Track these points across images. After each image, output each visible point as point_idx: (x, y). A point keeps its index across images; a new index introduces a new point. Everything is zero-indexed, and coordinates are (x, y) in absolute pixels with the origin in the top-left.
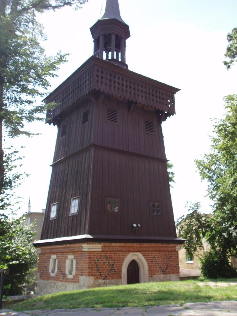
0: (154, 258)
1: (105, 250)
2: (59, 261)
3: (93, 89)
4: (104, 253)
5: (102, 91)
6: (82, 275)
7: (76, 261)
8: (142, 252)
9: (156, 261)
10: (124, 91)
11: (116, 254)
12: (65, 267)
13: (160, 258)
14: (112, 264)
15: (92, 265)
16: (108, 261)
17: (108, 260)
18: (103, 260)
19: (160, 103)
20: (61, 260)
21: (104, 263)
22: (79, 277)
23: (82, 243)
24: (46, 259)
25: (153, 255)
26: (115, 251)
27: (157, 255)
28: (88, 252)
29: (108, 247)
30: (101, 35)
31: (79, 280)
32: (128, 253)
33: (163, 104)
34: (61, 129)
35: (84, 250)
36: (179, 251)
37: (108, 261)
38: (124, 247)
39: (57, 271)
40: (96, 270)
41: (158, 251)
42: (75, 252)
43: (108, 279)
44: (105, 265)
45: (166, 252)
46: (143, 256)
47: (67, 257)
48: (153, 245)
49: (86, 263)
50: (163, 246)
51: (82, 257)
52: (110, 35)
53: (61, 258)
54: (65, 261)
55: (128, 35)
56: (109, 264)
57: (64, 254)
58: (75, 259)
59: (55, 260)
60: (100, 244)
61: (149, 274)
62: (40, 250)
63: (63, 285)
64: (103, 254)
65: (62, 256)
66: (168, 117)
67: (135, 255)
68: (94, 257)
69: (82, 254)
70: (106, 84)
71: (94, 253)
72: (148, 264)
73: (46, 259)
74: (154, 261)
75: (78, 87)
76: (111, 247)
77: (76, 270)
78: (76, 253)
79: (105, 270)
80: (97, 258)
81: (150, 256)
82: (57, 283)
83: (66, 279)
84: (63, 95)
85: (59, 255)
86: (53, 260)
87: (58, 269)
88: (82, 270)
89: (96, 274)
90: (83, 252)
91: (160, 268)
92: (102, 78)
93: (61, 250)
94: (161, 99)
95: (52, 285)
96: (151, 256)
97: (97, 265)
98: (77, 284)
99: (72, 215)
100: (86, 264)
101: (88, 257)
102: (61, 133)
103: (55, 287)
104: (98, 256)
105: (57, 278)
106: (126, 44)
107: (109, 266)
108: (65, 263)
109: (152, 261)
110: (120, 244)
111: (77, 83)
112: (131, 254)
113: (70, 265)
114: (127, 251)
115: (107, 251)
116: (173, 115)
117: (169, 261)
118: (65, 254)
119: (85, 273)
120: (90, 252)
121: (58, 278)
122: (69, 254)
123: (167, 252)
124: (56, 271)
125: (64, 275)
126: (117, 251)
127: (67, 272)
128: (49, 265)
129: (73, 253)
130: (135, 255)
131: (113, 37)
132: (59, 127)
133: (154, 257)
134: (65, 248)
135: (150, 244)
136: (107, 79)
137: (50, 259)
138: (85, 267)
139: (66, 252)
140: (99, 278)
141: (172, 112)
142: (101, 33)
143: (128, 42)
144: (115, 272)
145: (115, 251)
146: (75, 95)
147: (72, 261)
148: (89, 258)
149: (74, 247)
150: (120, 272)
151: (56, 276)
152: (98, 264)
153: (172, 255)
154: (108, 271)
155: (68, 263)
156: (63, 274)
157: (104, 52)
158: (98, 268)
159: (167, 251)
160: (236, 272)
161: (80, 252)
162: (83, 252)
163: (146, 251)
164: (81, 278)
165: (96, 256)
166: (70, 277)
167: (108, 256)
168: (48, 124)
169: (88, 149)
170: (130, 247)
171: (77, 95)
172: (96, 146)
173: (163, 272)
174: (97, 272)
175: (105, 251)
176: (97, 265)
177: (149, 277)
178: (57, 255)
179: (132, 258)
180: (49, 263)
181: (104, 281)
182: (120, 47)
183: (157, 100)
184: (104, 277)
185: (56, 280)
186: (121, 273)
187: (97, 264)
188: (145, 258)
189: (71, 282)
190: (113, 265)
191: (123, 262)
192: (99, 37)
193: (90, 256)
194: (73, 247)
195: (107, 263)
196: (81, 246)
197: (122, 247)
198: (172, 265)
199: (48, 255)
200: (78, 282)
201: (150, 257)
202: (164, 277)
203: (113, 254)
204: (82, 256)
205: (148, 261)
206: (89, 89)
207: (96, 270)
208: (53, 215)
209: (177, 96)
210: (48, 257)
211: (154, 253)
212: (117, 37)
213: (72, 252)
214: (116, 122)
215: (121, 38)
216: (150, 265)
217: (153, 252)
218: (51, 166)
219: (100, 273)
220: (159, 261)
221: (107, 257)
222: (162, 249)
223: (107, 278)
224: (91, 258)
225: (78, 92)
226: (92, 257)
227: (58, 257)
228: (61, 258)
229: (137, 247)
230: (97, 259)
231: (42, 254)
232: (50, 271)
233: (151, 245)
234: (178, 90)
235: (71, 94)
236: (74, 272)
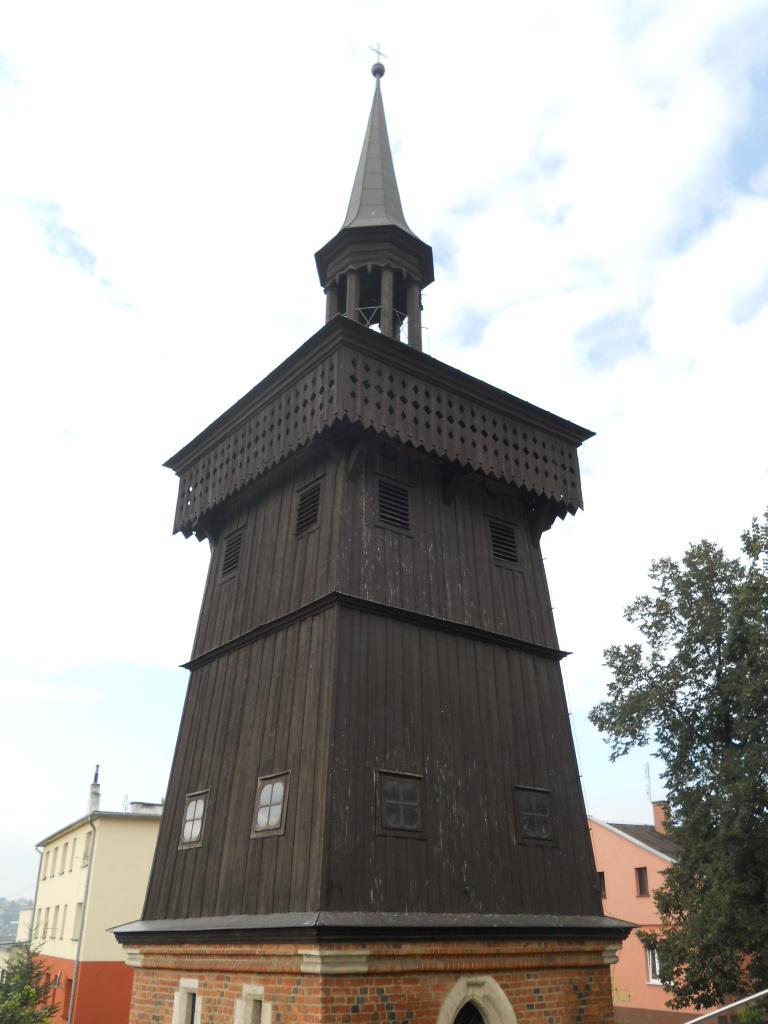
0: (537, 995)
2: (209, 1001)
3: (341, 418)
5: (367, 425)
7: (275, 1008)
8: (499, 974)
9: (543, 1006)
10: (433, 428)
13: (554, 993)
19: (537, 470)
20: (217, 997)
23: (300, 946)
25: (533, 983)
30: (350, 270)
32: (453, 977)
33: (547, 474)
34: (223, 553)
36: (612, 966)
42: (271, 973)
46: (503, 987)
47: (239, 989)
48: (534, 946)
51: (299, 995)
52: (377, 271)
53: (215, 993)
54: (232, 1004)
55: (428, 278)
57: (228, 979)
58: (268, 999)
59: (194, 995)
60: (364, 947)
64: (370, 982)
65: (219, 982)
66: (558, 519)
68: (340, 996)
69: (299, 983)
73: (162, 990)
75: (288, 417)
78: (273, 977)
80: (350, 1000)
81: (523, 988)
84: (236, 442)
85: (210, 978)
86: (186, 996)
90: (303, 974)
93: (216, 963)
94: (540, 460)
96: (528, 988)
99: (260, 835)
102: (222, 562)
106: (423, 302)
108: (231, 1012)
109: (530, 1007)
110: (429, 946)
111: (283, 403)
112: (463, 981)
116: (573, 512)
118: (231, 976)
122: (247, 981)
128: (169, 1013)
129: (261, 977)
131: (387, 281)
132: (214, 543)
133: (537, 991)
134: (236, 955)
135: (523, 944)
136: (381, 391)
137: (172, 991)
141: (568, 502)
142: (351, 267)
143: (428, 294)
146: (275, 439)
147: (258, 1004)
162: (299, 977)
167: (388, 990)
168: (180, 534)
169: (315, 609)
171: (282, 438)
172: (348, 604)
178: (201, 978)
179: (466, 996)
180: (171, 1005)
182: (407, 304)
183: (518, 467)
188: (508, 994)
191: (437, 1013)
192: (343, 279)
199: (168, 977)
201: (524, 992)
203: (407, 982)
204: (296, 991)
206: (325, 418)
208: (192, 830)
209: (585, 452)
210: (169, 984)
212: (397, 275)
213: (259, 973)
214: (407, 525)
215: (409, 279)
217: (532, 973)
220: (550, 1006)
221: (385, 994)
222: (560, 961)
224: (331, 1001)
225: (288, 431)
228: (215, 993)
230: (351, 1005)
233: (525, 946)
234: (588, 434)
235: (261, 439)
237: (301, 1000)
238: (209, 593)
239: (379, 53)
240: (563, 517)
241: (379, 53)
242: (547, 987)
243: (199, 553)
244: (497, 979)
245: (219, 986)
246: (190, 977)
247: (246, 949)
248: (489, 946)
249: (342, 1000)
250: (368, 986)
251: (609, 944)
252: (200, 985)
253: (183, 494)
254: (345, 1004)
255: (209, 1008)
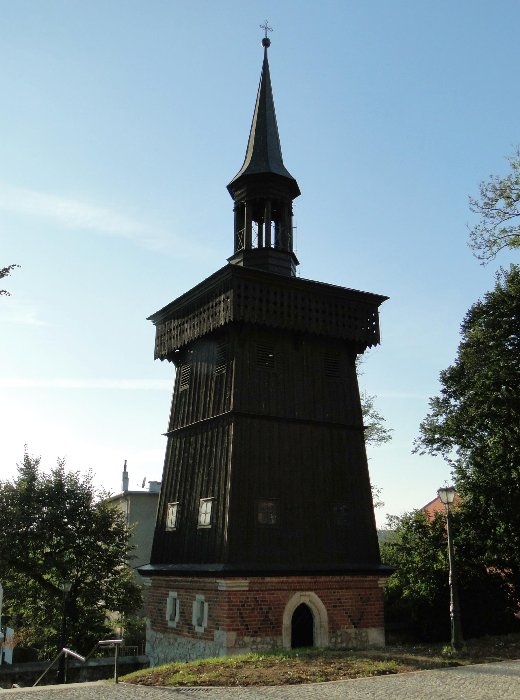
1: (254, 588)
4: (253, 593)
6: (218, 629)
7: (209, 605)
8: (317, 591)
11: (273, 594)
12: (191, 614)
14: (266, 611)
15: (233, 613)
16: (259, 607)
17: (260, 605)
18: (250, 605)
21: (253, 609)
22: (213, 632)
24: (161, 596)
25: (337, 596)
26: (272, 590)
27: (345, 595)
28: (227, 593)
29: (259, 583)
31: (213, 636)
32: (293, 592)
35: (219, 588)
37: (259, 607)
38: (286, 582)
39: (180, 619)
40: (240, 621)
41: (346, 588)
42: (207, 590)
43: (260, 636)
44: (254, 613)
45: (360, 590)
46: (319, 597)
47: (195, 597)
49: (224, 610)
50: (354, 579)
54: (192, 603)
56: (261, 611)
58: (206, 601)
60: (247, 579)
61: (330, 628)
62: (151, 581)
63: (190, 642)
67: (305, 596)
70: (253, 308)
71: (235, 594)
72: (328, 610)
73: (161, 596)
74: (339, 606)
76: (264, 583)
77: (208, 619)
78: (208, 592)
79: (255, 621)
80: (241, 602)
82: (178, 639)
83: (193, 633)
85: (182, 592)
87: (181, 616)
88: (218, 620)
89: (239, 627)
90: (219, 591)
91: (350, 616)
92: (246, 297)
95: (171, 641)
97: (241, 613)
98: (211, 643)
100: (224, 612)
101: (227, 600)
103: (177, 645)
104: (243, 598)
105: (178, 631)
107: (261, 614)
108: (191, 607)
112: (298, 594)
113: (199, 611)
114: (291, 589)
115: (257, 591)
117: (367, 605)
118: (191, 591)
119: (222, 625)
120: (230, 592)
121: (180, 631)
122: (197, 593)
123: (363, 590)
124: (177, 618)
125: (191, 628)
126: (275, 590)
127: (194, 622)
130: (305, 596)
133: (339, 599)
134: (192, 582)
135: (330, 577)
138: (223, 617)
139: (193, 589)
140: (245, 635)
141: (374, 339)
144: (271, 623)
145: (272, 590)
148: (227, 602)
149: (205, 582)
150: (279, 623)
151: (177, 626)
152: (243, 612)
153: (371, 594)
154: (260, 623)
155: (196, 606)
156: (188, 624)
157: (253, 223)
158: (242, 617)
159: (362, 588)
160: (517, 619)
161: (215, 590)
163: (324, 589)
164: (217, 633)
165: (240, 598)
166: (200, 630)
167: (259, 598)
170: (295, 583)
173: (354, 624)
174: (242, 625)
175: (254, 591)
176: (241, 613)
177: (330, 632)
178: (178, 592)
180: (166, 604)
181: (252, 639)
184: (252, 632)
185: (178, 634)
186: (281, 627)
187: (241, 611)
188: (322, 600)
189: (200, 638)
190: (268, 613)
191: (284, 608)
193: (229, 598)
194: (203, 582)
195: (257, 609)
196: (216, 582)
197: (282, 583)
198: (371, 612)
199: (164, 591)
200: (212, 640)
201: (332, 600)
202: (356, 633)
203: (268, 594)
204: (217, 598)
205: (328, 605)
207: (240, 621)
210: (164, 594)
211: (339, 592)
216: (331, 612)
218: (165, 435)
219: (246, 625)
220: (346, 606)
221: (258, 599)
223: (258, 633)
224: (232, 602)
226: (234, 600)
227: (180, 595)
229: (308, 582)
230: (241, 604)
231: (155, 587)
232: (168, 618)
233: (332, 578)
236: (205, 624)
237: (219, 602)
238: (176, 395)
239: (266, 28)
240: (370, 347)
241: (266, 28)
242: (345, 597)
243: (168, 370)
244: (316, 593)
245: (186, 595)
246: (173, 591)
247: (196, 579)
248: (311, 578)
249: (237, 602)
250: (249, 596)
251: (381, 577)
252: (178, 595)
253: (159, 336)
254: (238, 603)
255: (182, 604)
